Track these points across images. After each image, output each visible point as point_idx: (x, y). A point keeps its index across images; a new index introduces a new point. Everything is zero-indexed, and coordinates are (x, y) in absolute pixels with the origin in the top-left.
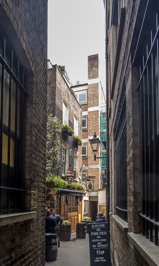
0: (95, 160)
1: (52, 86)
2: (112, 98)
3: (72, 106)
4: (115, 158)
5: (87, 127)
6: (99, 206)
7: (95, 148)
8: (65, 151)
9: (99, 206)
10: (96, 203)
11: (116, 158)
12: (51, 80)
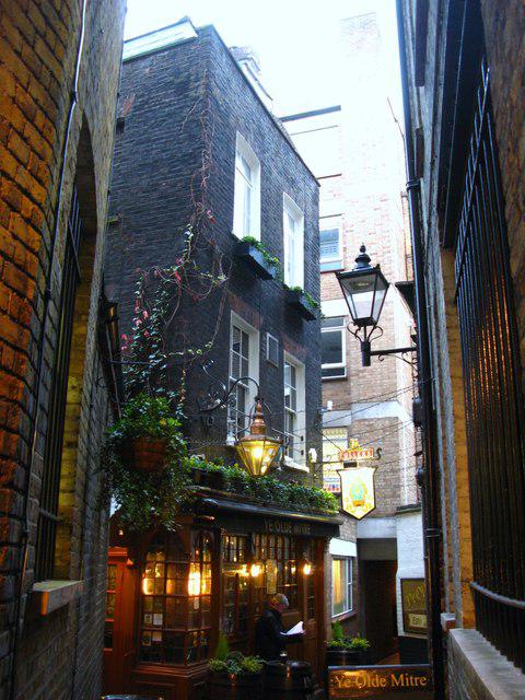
0: (367, 362)
1: (192, 94)
2: (421, 81)
3: (275, 171)
4: (452, 331)
5: (345, 257)
6: (402, 580)
7: (364, 313)
8: (246, 337)
9: (402, 580)
10: (392, 565)
11: (457, 334)
12: (190, 75)
